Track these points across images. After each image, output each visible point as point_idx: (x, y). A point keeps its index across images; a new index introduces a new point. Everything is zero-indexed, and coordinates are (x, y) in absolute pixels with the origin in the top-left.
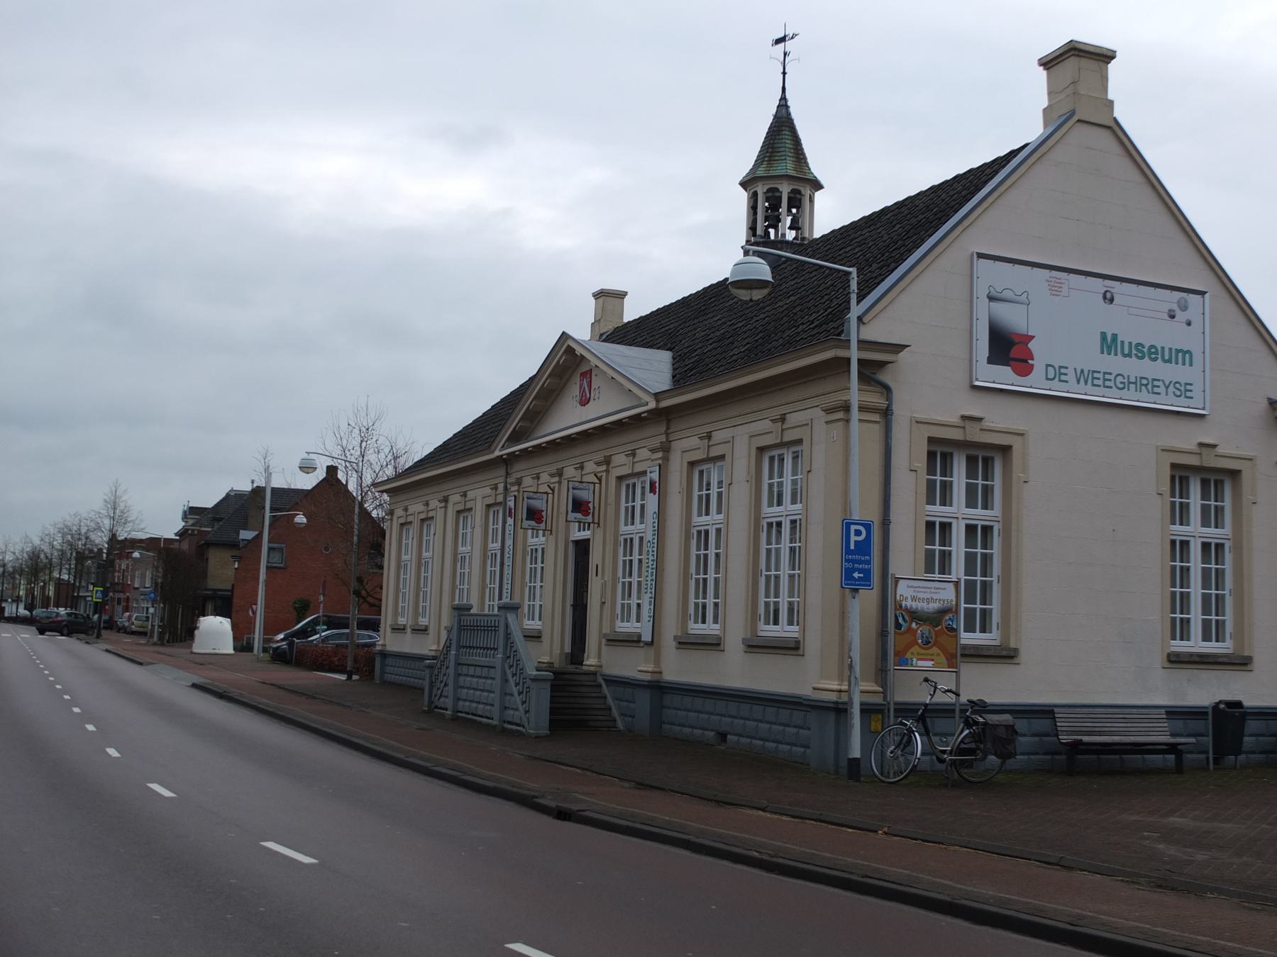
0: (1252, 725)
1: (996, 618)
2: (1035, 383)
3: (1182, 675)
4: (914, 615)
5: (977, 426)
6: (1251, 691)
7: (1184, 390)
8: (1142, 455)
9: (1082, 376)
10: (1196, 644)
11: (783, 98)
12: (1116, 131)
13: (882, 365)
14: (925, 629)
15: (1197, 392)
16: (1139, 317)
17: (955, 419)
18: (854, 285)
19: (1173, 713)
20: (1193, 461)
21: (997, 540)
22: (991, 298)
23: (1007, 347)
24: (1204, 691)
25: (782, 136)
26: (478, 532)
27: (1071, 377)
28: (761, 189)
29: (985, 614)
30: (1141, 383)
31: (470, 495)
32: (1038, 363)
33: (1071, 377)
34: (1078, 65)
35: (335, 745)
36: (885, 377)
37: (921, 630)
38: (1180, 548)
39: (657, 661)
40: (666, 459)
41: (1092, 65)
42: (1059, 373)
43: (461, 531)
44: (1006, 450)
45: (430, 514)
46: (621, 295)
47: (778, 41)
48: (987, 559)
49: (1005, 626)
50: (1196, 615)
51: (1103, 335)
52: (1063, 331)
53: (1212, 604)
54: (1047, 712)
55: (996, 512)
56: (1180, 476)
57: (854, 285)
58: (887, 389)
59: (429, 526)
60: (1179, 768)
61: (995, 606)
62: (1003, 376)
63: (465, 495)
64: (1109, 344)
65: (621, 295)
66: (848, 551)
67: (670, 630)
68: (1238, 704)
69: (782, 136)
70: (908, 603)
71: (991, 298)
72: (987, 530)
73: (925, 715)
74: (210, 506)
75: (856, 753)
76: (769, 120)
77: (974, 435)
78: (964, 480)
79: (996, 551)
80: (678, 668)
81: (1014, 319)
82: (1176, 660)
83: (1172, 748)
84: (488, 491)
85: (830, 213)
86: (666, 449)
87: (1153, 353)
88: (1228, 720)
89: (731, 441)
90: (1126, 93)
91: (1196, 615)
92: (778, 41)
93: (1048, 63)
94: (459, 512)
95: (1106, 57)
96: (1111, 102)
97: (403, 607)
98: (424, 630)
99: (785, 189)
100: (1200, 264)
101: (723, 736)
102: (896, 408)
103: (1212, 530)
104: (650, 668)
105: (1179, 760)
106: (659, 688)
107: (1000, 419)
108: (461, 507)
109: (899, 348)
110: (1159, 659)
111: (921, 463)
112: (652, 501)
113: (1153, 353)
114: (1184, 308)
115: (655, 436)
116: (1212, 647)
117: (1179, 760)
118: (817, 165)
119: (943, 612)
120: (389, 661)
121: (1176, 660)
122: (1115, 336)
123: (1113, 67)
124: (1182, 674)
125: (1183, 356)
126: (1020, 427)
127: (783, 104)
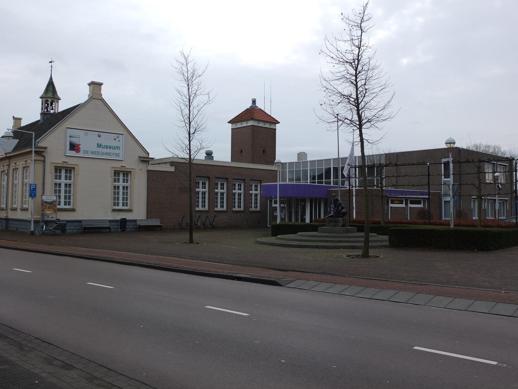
0: (128, 223)
1: (72, 203)
2: (81, 154)
3: (116, 213)
4: (46, 202)
5: (66, 164)
6: (129, 216)
7: (118, 155)
8: (107, 169)
9: (92, 153)
10: (121, 207)
11: (51, 77)
12: (103, 100)
13: (43, 152)
14: (49, 205)
15: (121, 155)
16: (107, 140)
17: (61, 162)
18: (34, 136)
19: (110, 221)
20: (120, 170)
21: (72, 187)
22: (70, 137)
23: (74, 147)
24: (119, 217)
25: (51, 85)
26: (21, 176)
27: (90, 153)
28: (44, 100)
29: (127, 203)
30: (107, 154)
31: (18, 164)
32: (82, 150)
33: (90, 153)
34: (95, 86)
35: (146, 269)
36: (44, 154)
37: (48, 205)
38: (116, 188)
39: (7, 213)
40: (9, 168)
41: (98, 86)
42: (87, 152)
43: (25, 174)
44: (74, 168)
45: (28, 165)
46: (20, 119)
47: (51, 62)
48: (127, 193)
49: (130, 205)
50: (121, 201)
51: (98, 144)
52: (88, 143)
53: (125, 199)
54: (80, 221)
55: (129, 184)
56: (117, 173)
57: (34, 136)
58: (44, 156)
59: (16, 172)
60: (110, 232)
61: (72, 200)
62: (73, 153)
63: (16, 163)
64: (99, 146)
65: (20, 119)
66: (31, 190)
67: (10, 206)
68: (125, 219)
69: (51, 85)
70: (45, 200)
71: (70, 137)
72: (70, 185)
73: (47, 222)
74: (86, 98)
75: (32, 230)
76: (47, 82)
77: (65, 165)
78: (64, 174)
79: (72, 189)
80: (12, 215)
81: (75, 141)
82: (114, 210)
83: (109, 228)
84: (24, 162)
85: (62, 106)
86: (9, 165)
87: (110, 147)
88: (124, 222)
89: (19, 165)
90: (106, 93)
91: (121, 201)
92: (51, 62)
93: (89, 85)
94: (24, 167)
95: (101, 84)
96: (102, 94)
97: (15, 201)
98: (27, 210)
99: (50, 100)
100: (123, 128)
101: (17, 229)
102: (46, 160)
103: (68, 181)
104: (5, 215)
105: (110, 231)
106: (7, 220)
107: (71, 162)
108: (14, 168)
109: (46, 148)
110: (110, 210)
111: (53, 171)
112: (6, 177)
113: (110, 147)
114: (118, 137)
115: (6, 162)
116: (125, 208)
117: (110, 231)
118: (59, 93)
119: (53, 202)
120: (10, 222)
121: (114, 210)
122: (101, 144)
123: (102, 86)
124: (116, 213)
125: (118, 148)
126: (77, 164)
127: (51, 78)
